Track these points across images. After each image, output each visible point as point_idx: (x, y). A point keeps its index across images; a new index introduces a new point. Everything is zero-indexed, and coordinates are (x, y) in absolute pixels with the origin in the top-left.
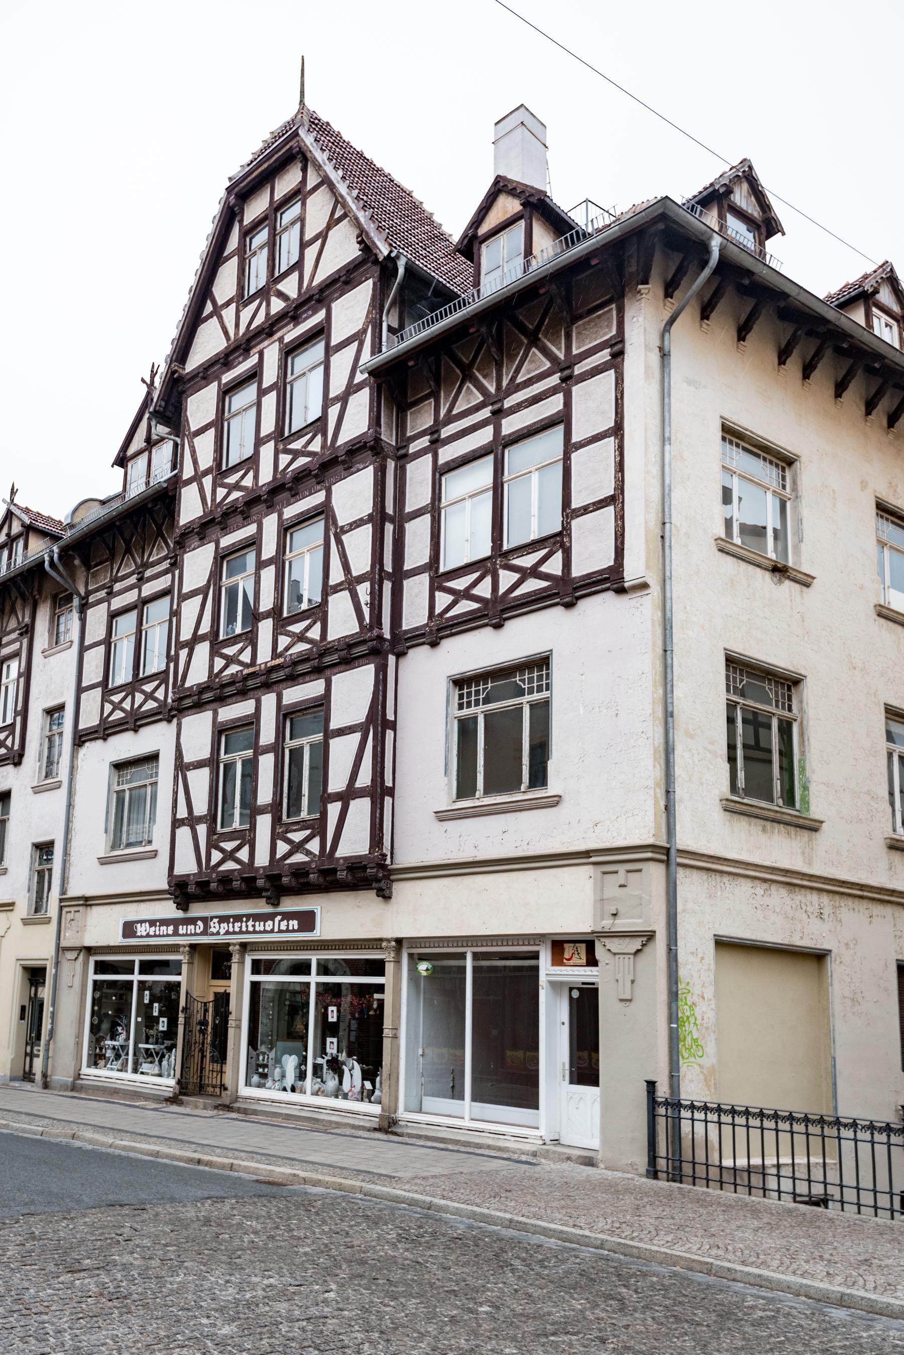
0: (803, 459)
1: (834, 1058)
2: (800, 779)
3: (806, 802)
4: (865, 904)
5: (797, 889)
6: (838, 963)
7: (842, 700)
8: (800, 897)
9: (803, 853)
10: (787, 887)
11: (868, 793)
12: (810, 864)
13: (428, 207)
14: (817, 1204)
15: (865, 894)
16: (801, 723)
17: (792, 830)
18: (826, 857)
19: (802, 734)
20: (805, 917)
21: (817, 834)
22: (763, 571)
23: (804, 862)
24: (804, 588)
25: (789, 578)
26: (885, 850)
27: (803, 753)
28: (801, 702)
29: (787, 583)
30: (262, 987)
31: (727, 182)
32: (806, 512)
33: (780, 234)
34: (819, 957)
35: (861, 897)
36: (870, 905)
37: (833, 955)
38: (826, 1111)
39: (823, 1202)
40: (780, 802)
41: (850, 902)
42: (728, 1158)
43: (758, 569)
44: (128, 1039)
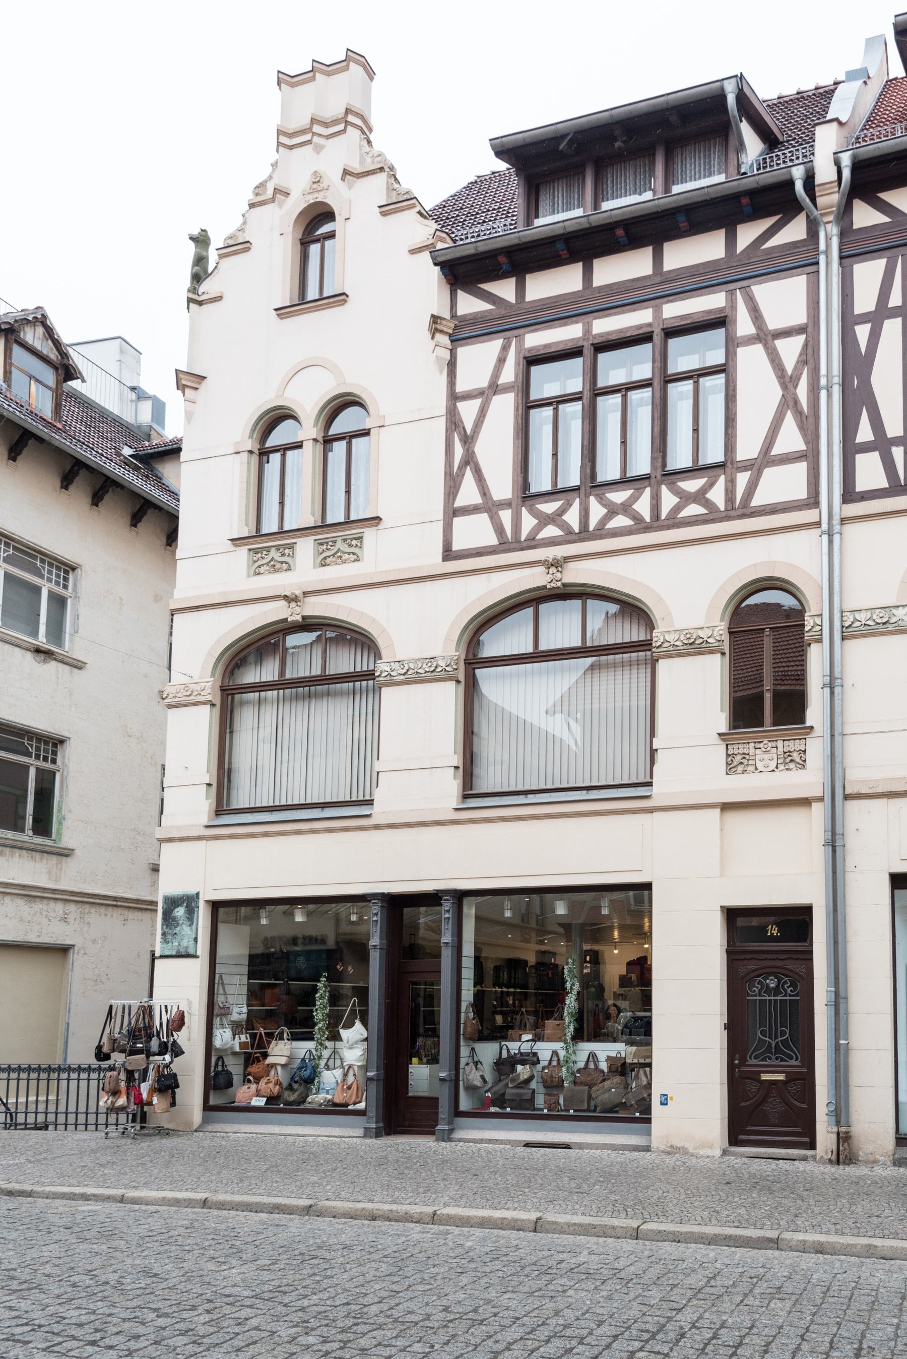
0: (85, 568)
1: (68, 1024)
2: (58, 817)
3: (59, 834)
4: (120, 911)
5: (38, 900)
6: (81, 954)
7: (112, 759)
8: (39, 906)
9: (49, 873)
10: (26, 898)
11: (134, 830)
12: (57, 880)
13: (790, 90)
14: (40, 1129)
15: (119, 903)
16: (62, 775)
17: (38, 855)
18: (70, 877)
19: (62, 782)
20: (45, 921)
21: (69, 859)
22: (23, 651)
23: (50, 879)
24: (76, 670)
25: (55, 659)
26: (150, 872)
27: (61, 796)
28: (64, 757)
29: (54, 663)
30: (259, 951)
31: (12, 321)
32: (83, 611)
33: (79, 380)
34: (64, 950)
35: (116, 906)
36: (126, 912)
37: (76, 948)
38: (58, 1061)
39: (46, 1127)
40: (31, 833)
41: (102, 910)
42: (22, 1103)
43: (17, 649)
44: (790, 995)
